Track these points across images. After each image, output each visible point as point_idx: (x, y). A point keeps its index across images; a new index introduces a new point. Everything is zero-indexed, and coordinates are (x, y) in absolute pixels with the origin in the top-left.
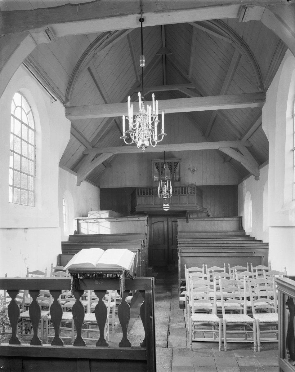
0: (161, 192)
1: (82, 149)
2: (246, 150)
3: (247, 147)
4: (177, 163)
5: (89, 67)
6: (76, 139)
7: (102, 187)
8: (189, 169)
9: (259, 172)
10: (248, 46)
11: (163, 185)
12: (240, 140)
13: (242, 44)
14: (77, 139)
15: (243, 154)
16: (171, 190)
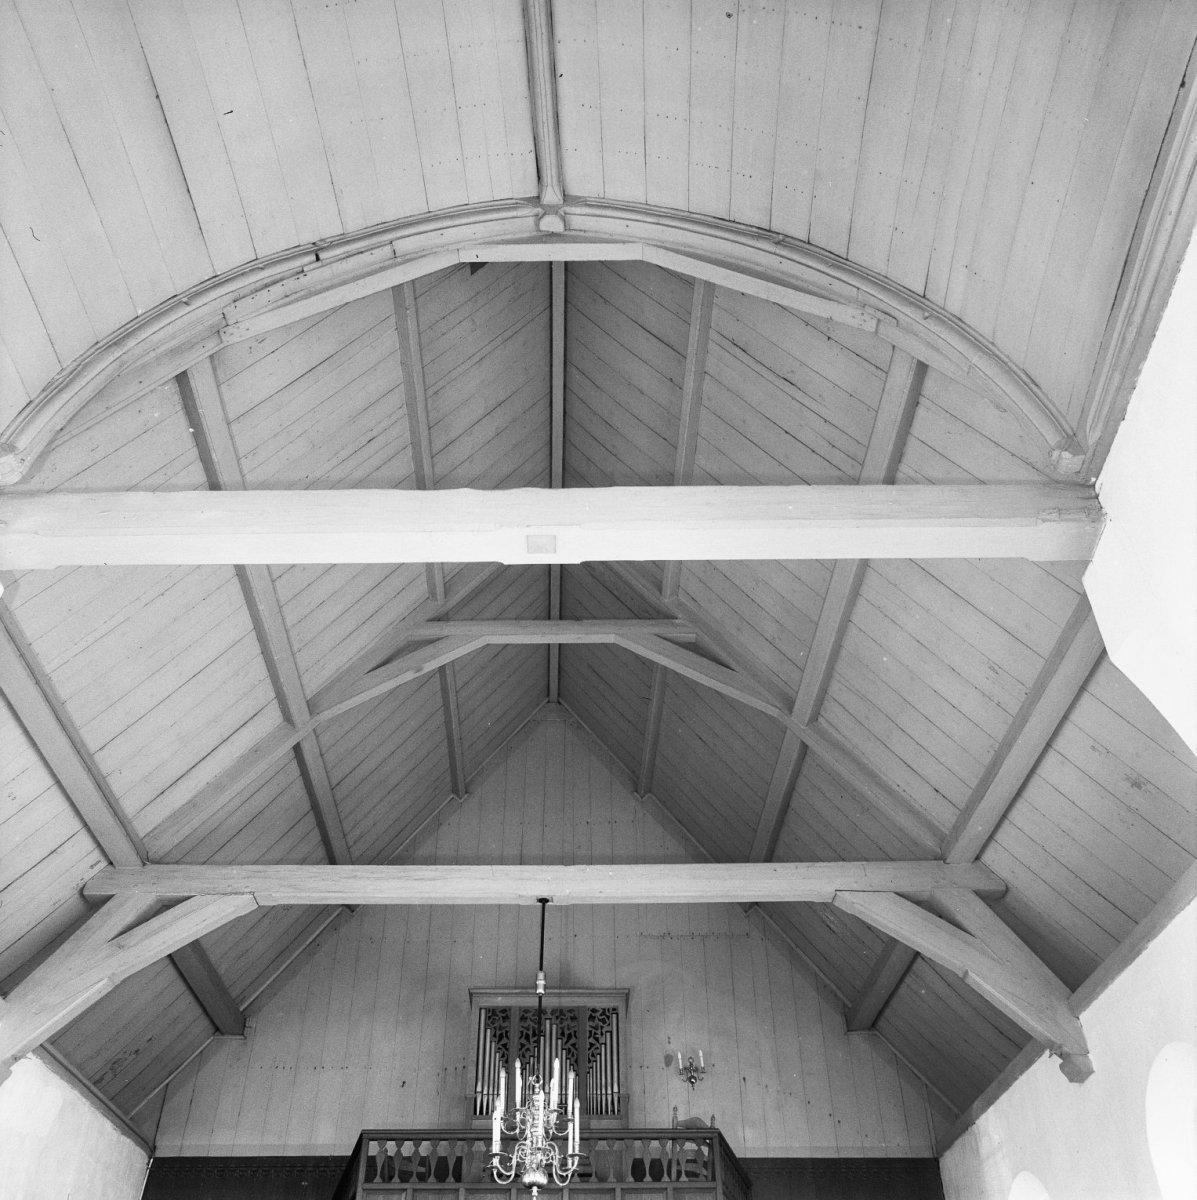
0: (509, 1141)
1: (79, 863)
2: (980, 907)
3: (982, 895)
4: (603, 1013)
5: (298, 744)
6: (184, 988)
7: (168, 1148)
8: (669, 1060)
9: (1079, 1030)
10: (960, 319)
11: (528, 1089)
12: (941, 858)
13: (926, 314)
14: (58, 782)
15: (971, 928)
16: (574, 1131)
